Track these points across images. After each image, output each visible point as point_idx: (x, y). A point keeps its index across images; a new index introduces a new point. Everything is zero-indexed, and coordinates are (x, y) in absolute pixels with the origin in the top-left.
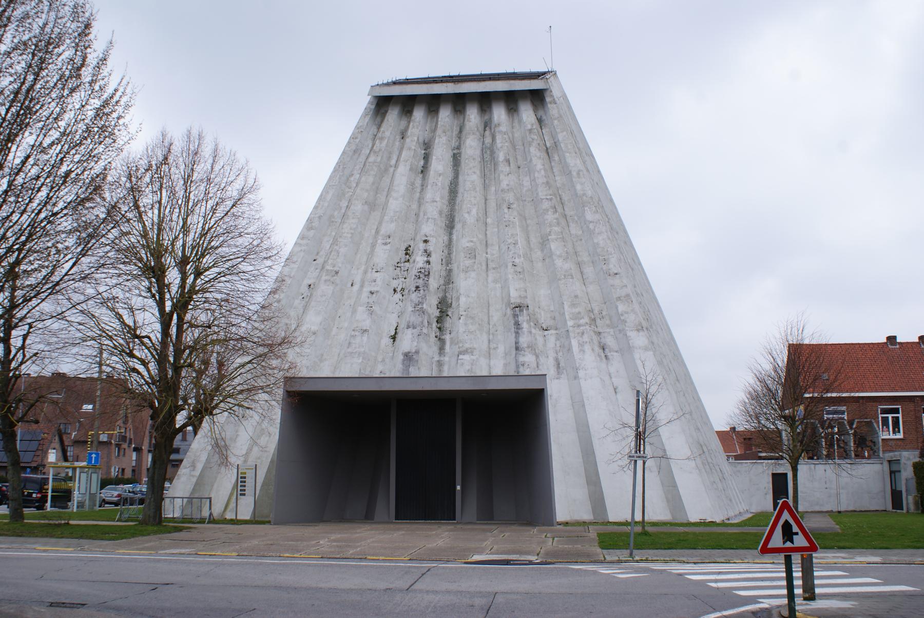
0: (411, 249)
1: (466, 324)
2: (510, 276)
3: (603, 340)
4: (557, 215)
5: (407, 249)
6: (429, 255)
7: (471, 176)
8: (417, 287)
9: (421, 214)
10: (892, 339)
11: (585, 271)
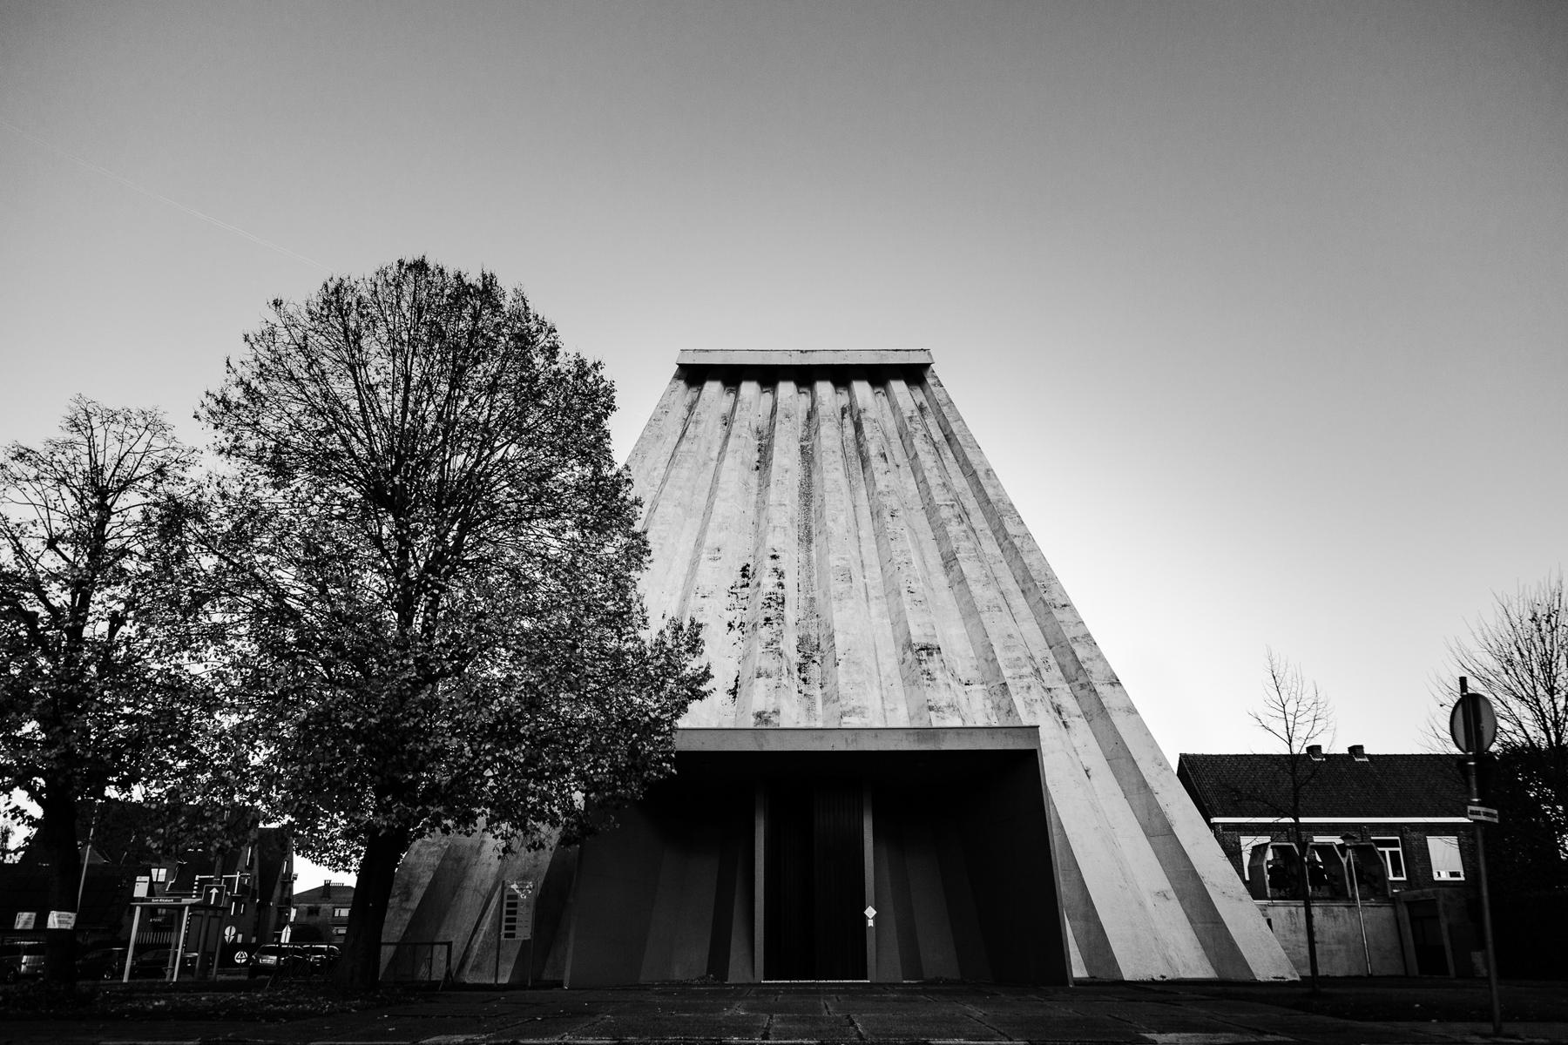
0: (751, 569)
1: (847, 672)
2: (907, 607)
3: (1056, 700)
4: (964, 527)
5: (744, 569)
6: (781, 575)
7: (833, 472)
8: (768, 619)
9: (763, 522)
10: (1356, 750)
11: (1013, 604)
